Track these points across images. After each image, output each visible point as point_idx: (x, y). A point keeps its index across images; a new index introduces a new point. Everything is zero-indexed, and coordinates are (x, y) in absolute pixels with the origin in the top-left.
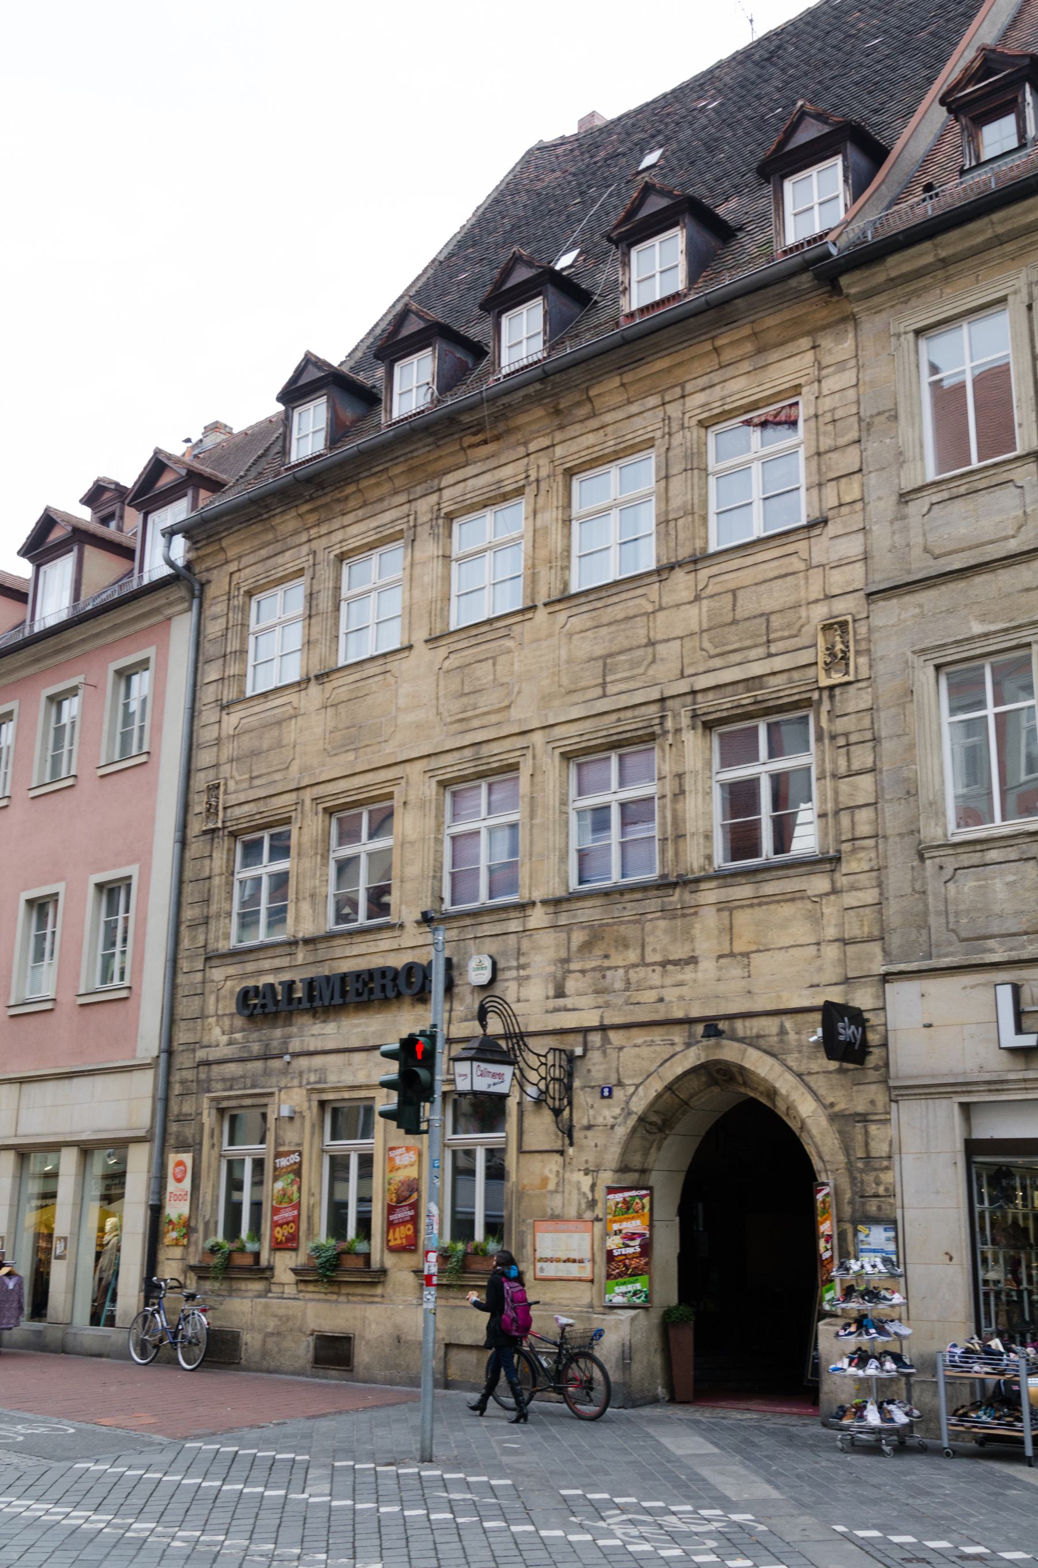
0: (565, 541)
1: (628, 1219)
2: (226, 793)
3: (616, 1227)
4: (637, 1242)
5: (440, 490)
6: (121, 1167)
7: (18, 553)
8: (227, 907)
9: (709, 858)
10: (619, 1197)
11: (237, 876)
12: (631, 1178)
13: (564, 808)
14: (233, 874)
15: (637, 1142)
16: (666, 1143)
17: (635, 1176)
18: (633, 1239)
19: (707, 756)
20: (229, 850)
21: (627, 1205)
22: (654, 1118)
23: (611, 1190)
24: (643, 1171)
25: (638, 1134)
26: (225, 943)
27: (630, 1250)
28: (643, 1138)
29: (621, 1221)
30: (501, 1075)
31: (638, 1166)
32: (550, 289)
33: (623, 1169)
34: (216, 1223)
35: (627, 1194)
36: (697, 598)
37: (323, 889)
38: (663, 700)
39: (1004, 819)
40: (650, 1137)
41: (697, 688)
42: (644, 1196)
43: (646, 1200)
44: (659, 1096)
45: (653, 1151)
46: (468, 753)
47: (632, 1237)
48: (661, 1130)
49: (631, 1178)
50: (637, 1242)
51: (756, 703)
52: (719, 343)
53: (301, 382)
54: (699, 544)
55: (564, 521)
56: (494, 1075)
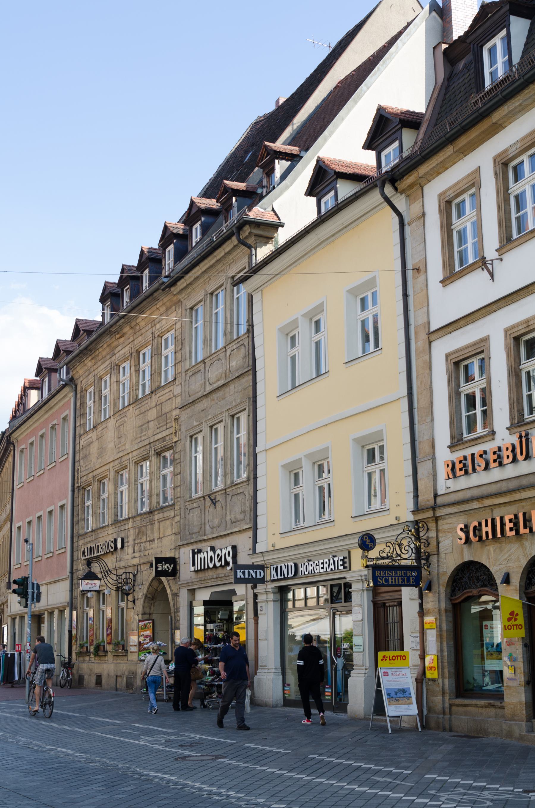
0: (137, 378)
1: (145, 631)
2: (81, 472)
3: (142, 633)
4: (148, 639)
5: (115, 354)
6: (460, 597)
7: (305, 195)
8: (83, 517)
9: (158, 503)
10: (143, 623)
11: (86, 504)
12: (147, 616)
13: (136, 483)
14: (84, 504)
15: (146, 604)
16: (156, 604)
17: (148, 616)
18: (147, 638)
19: (158, 465)
20: (82, 494)
21: (145, 626)
22: (149, 596)
23: (140, 621)
24: (150, 614)
25: (146, 602)
26: (83, 531)
27: (146, 641)
28: (148, 602)
29: (143, 632)
30: (95, 584)
31: (148, 613)
32: (150, 264)
33: (144, 614)
34: (83, 636)
35: (145, 622)
36: (156, 405)
37: (98, 511)
38: (150, 444)
39: (374, 449)
40: (151, 602)
41: (151, 441)
42: (150, 623)
43: (151, 624)
44: (148, 588)
45: (152, 607)
46: (117, 462)
47: (147, 637)
48: (153, 599)
49: (147, 616)
50: (148, 639)
51: (164, 446)
52: (158, 306)
53: (105, 294)
54: (158, 384)
55: (136, 371)
56: (92, 584)
